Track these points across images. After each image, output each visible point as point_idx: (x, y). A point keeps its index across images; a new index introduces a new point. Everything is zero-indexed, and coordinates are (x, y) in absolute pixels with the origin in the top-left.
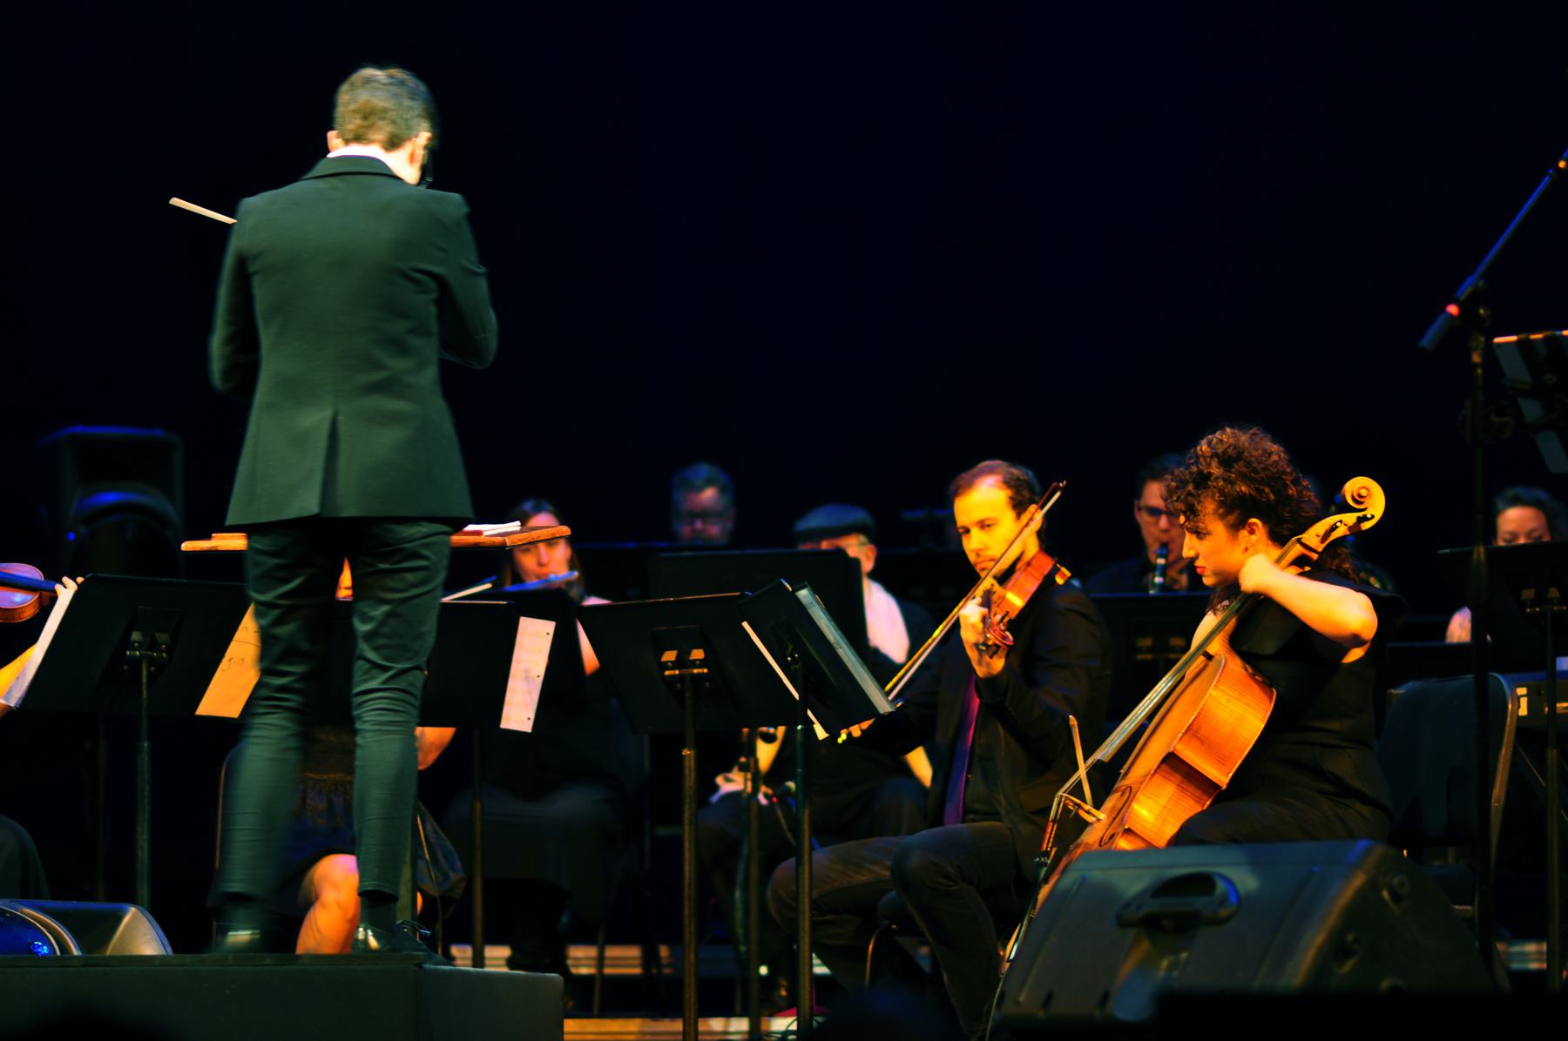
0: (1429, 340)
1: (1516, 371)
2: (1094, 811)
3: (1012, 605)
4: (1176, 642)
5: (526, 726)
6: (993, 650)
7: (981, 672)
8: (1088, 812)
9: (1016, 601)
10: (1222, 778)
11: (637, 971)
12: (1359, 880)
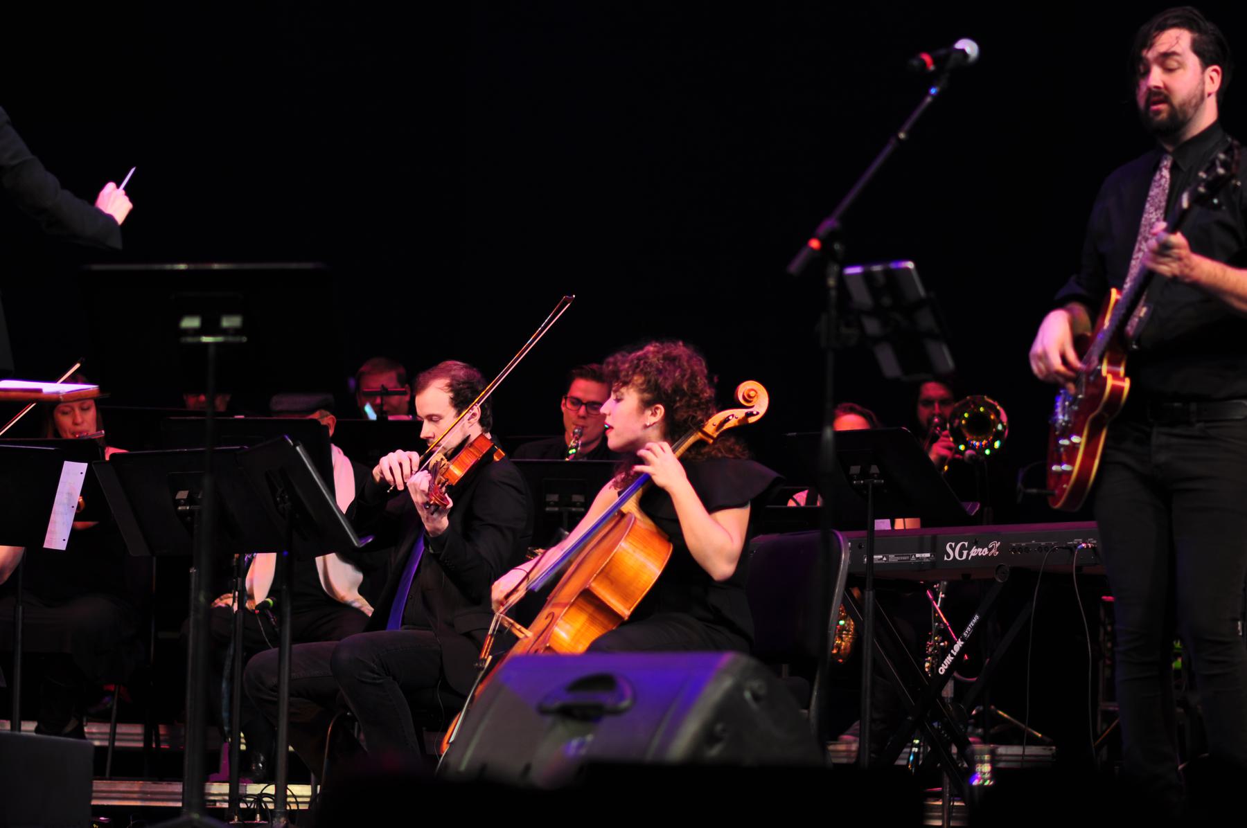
0: (795, 267)
1: (861, 297)
2: (523, 629)
3: (452, 474)
4: (577, 498)
5: (62, 546)
6: (438, 509)
7: (428, 526)
8: (519, 630)
9: (457, 472)
10: (625, 611)
11: (141, 745)
12: (728, 683)
